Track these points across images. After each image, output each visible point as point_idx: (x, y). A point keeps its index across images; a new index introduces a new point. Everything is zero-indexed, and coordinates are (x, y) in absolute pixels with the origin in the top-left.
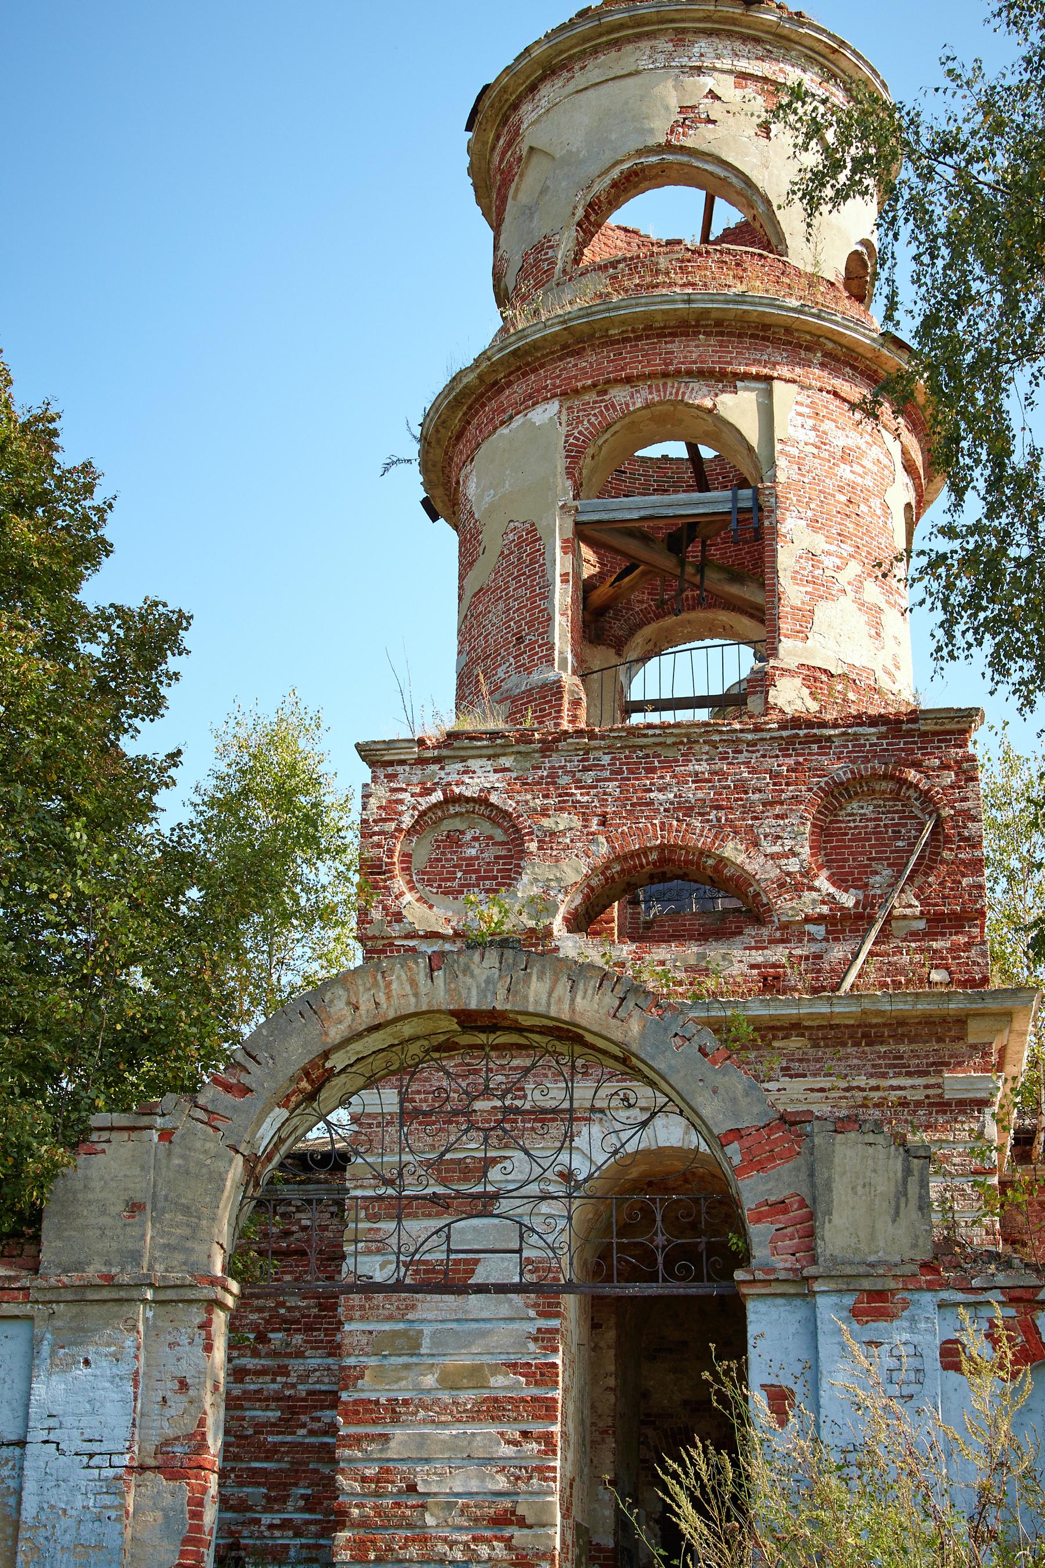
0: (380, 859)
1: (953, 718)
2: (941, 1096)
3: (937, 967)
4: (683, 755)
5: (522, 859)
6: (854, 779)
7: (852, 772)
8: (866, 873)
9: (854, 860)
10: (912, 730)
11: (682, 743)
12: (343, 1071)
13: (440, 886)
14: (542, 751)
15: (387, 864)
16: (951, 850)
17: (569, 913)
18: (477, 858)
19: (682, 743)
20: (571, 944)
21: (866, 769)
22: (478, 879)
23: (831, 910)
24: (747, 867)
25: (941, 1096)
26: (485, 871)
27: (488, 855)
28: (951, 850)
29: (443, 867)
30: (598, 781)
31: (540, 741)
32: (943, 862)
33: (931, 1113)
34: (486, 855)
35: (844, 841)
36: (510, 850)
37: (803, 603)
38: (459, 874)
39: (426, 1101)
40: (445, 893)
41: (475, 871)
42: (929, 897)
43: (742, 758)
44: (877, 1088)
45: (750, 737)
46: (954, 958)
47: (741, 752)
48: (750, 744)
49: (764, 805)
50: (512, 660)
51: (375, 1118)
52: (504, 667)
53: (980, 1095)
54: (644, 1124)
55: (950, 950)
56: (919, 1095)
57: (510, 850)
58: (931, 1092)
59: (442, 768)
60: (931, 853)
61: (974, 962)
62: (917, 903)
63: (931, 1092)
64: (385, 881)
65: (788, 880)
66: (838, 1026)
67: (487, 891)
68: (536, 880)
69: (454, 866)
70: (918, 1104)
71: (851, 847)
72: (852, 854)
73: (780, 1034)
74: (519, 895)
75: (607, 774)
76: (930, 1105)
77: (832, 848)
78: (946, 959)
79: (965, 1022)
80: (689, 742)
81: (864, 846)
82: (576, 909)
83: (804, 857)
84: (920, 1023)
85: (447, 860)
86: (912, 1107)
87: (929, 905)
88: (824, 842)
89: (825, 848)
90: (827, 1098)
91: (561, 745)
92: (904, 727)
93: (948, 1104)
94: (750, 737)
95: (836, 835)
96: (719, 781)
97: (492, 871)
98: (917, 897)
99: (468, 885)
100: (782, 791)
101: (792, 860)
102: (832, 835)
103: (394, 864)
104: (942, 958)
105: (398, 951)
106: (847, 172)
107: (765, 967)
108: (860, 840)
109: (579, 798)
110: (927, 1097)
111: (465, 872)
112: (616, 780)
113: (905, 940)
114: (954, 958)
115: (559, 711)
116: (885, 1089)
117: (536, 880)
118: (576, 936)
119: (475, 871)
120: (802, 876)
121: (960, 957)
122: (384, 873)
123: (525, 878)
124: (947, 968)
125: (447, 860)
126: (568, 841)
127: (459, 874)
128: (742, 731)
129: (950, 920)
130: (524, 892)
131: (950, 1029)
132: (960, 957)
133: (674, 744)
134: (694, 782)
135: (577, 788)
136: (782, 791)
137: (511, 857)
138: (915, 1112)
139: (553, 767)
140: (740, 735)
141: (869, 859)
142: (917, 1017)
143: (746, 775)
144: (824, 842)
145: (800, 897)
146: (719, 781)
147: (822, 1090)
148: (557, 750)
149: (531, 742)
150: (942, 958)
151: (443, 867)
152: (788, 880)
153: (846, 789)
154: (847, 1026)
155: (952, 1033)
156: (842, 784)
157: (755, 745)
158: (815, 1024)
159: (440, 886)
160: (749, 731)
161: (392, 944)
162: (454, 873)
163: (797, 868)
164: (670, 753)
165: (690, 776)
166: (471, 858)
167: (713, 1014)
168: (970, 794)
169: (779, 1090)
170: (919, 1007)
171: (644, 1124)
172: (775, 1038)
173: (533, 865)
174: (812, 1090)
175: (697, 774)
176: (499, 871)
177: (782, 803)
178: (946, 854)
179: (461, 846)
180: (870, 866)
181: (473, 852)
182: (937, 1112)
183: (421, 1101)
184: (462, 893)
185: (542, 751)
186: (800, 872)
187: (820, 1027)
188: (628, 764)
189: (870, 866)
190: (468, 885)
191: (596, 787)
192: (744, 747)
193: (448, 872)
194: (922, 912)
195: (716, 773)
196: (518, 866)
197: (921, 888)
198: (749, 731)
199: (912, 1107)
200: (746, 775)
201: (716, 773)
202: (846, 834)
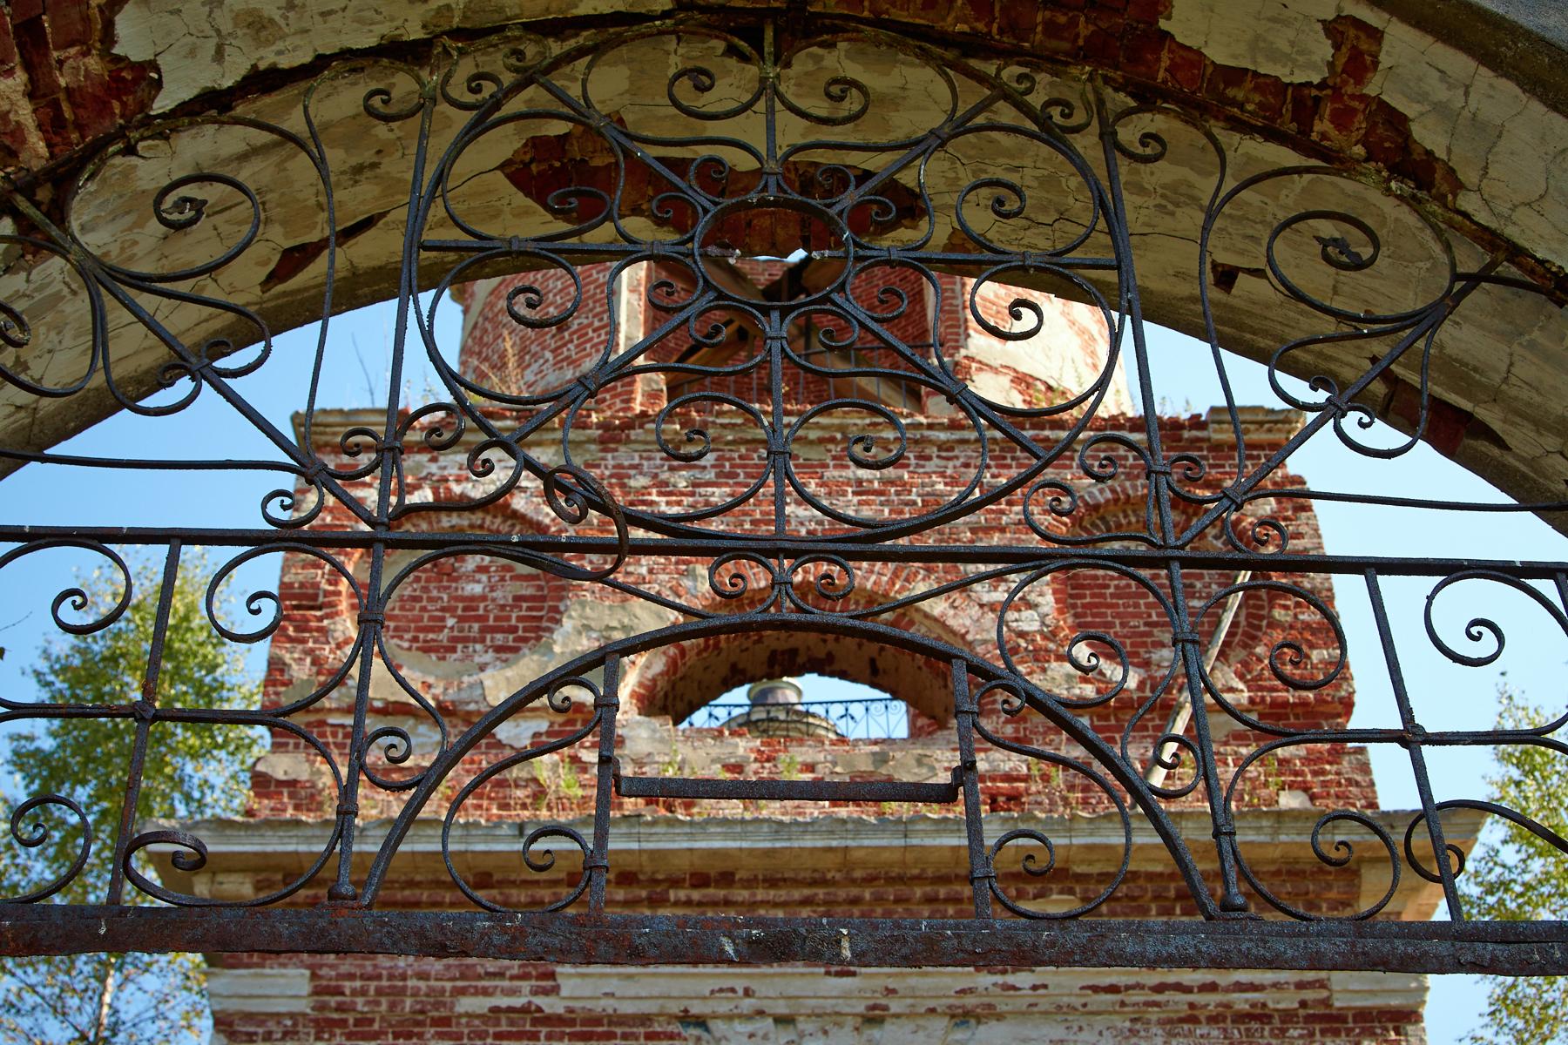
0: (316, 586)
1: (1261, 423)
2: (1326, 1003)
3: (1292, 786)
4: (834, 458)
5: (561, 599)
6: (1116, 500)
7: (1113, 491)
8: (1144, 644)
9: (1123, 625)
10: (1199, 440)
11: (832, 440)
12: (212, 105)
13: (415, 639)
14: (602, 441)
15: (327, 593)
16: (1286, 608)
17: (641, 684)
18: (483, 598)
19: (832, 440)
20: (644, 733)
21: (1135, 487)
22: (483, 630)
23: (1098, 691)
24: (951, 622)
25: (1326, 1003)
26: (497, 619)
27: (504, 594)
28: (1286, 608)
29: (424, 609)
30: (695, 485)
31: (599, 426)
32: (1273, 624)
33: (1312, 1034)
34: (498, 594)
35: (1103, 596)
36: (540, 588)
37: (996, 296)
38: (451, 622)
39: (363, 992)
40: (426, 650)
41: (478, 619)
42: (1260, 677)
43: (931, 466)
44: (1212, 987)
45: (943, 436)
46: (1315, 773)
47: (929, 458)
48: (942, 446)
49: (973, 531)
50: (548, 355)
51: (262, 1023)
52: (535, 367)
53: (1395, 1002)
54: (1194, 642)
55: (1306, 760)
56: (1289, 1001)
57: (540, 588)
58: (1309, 995)
59: (434, 460)
60: (1249, 616)
61: (1350, 782)
62: (1241, 686)
63: (1309, 995)
64: (320, 619)
65: (1023, 644)
66: (1135, 875)
67: (499, 649)
68: (587, 628)
69: (443, 609)
70: (1288, 1017)
71: (1117, 605)
72: (1118, 615)
73: (1031, 889)
74: (557, 649)
75: (710, 475)
76: (1310, 1019)
77: (1084, 606)
78: (1301, 773)
79: (1356, 873)
80: (845, 438)
81: (1137, 605)
82: (654, 680)
83: (1044, 610)
84: (1277, 873)
85: (430, 600)
86: (1276, 1022)
87: (1261, 688)
88: (1071, 596)
89: (1074, 606)
90: (1123, 1004)
91: (633, 434)
92: (1186, 434)
93: (1339, 1018)
94: (943, 436)
95: (1089, 587)
96: (898, 493)
97: (508, 618)
98: (1241, 677)
99: (465, 640)
100: (1003, 512)
101: (1026, 614)
102: (1083, 587)
103: (339, 593)
104: (1296, 774)
105: (335, 735)
106: (624, 693)
107: (993, 779)
108: (1129, 596)
109: (663, 508)
110: (1303, 1004)
111: (461, 619)
112: (727, 485)
113: (1226, 744)
114: (1315, 773)
115: (629, 401)
116: (1227, 990)
117: (587, 628)
118: (656, 722)
119: (478, 619)
120: (1045, 638)
121: (1324, 772)
122: (320, 608)
123: (568, 624)
124: (1306, 788)
125: (430, 600)
126: (644, 570)
127: (451, 622)
128: (930, 427)
129: (1297, 717)
130: (565, 645)
131: (1329, 887)
132: (1324, 772)
133: (821, 441)
134: (854, 493)
135: (660, 494)
136: (1003, 512)
137: (543, 599)
138: (1283, 1031)
139: (620, 466)
140: (927, 433)
141: (1146, 624)
142: (1273, 861)
143: (940, 487)
144: (1071, 596)
145: (1044, 670)
146: (898, 493)
147: (1113, 989)
148: (628, 441)
149: (585, 426)
150: (1296, 774)
151: (424, 609)
152: (1023, 644)
153: (1102, 519)
154: (1151, 876)
155: (1333, 895)
156: (1096, 507)
157: (951, 449)
158: (1095, 869)
159: (415, 639)
160: (942, 427)
161: (323, 723)
162: (443, 619)
163: (1035, 626)
164: (815, 454)
165: (848, 484)
166: (472, 598)
167: (915, 842)
168: (1303, 529)
169: (1035, 988)
170: (1283, 838)
171: (1194, 642)
172: (1021, 895)
173: (583, 604)
174: (1096, 989)
175: (859, 482)
176: (519, 619)
177: (1002, 530)
178: (1278, 614)
179: (456, 580)
180: (1149, 634)
181: (477, 589)
182: (1323, 1032)
183: (354, 993)
184: (454, 650)
185: (602, 441)
186: (1041, 632)
187: (1103, 877)
188: (744, 466)
189: (1149, 634)
190: (465, 640)
191: (692, 494)
192: (934, 451)
193: (431, 618)
194: (1252, 701)
195: (892, 483)
196: (556, 610)
197: (1245, 664)
198: (942, 427)
199: (1276, 1022)
200: (940, 487)
201: (892, 483)
202: (1107, 587)
